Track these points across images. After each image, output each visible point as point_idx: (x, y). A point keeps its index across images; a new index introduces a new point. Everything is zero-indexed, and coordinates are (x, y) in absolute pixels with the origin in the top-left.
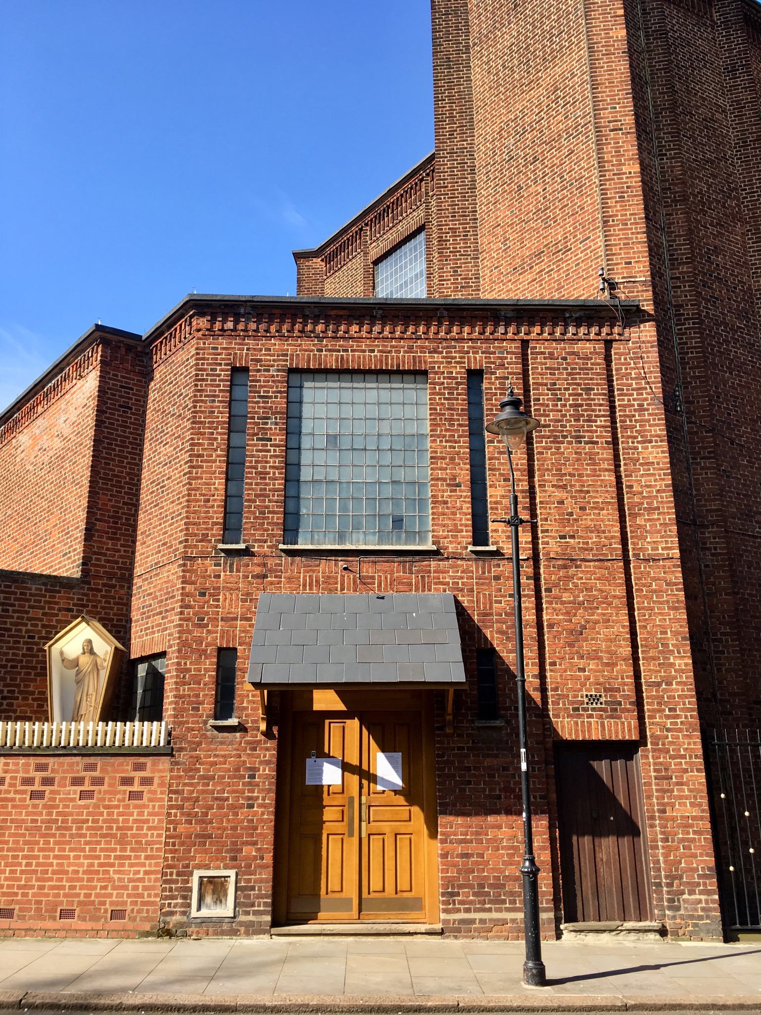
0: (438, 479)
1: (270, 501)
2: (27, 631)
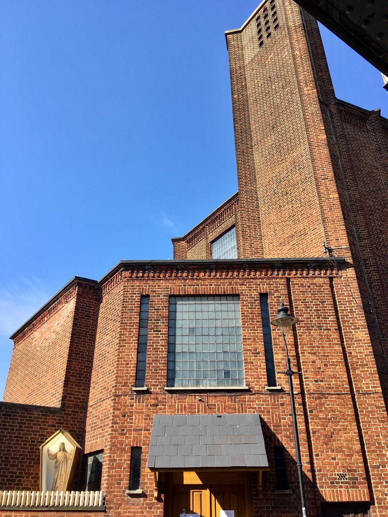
0: (247, 350)
1: (160, 363)
2: (31, 438)
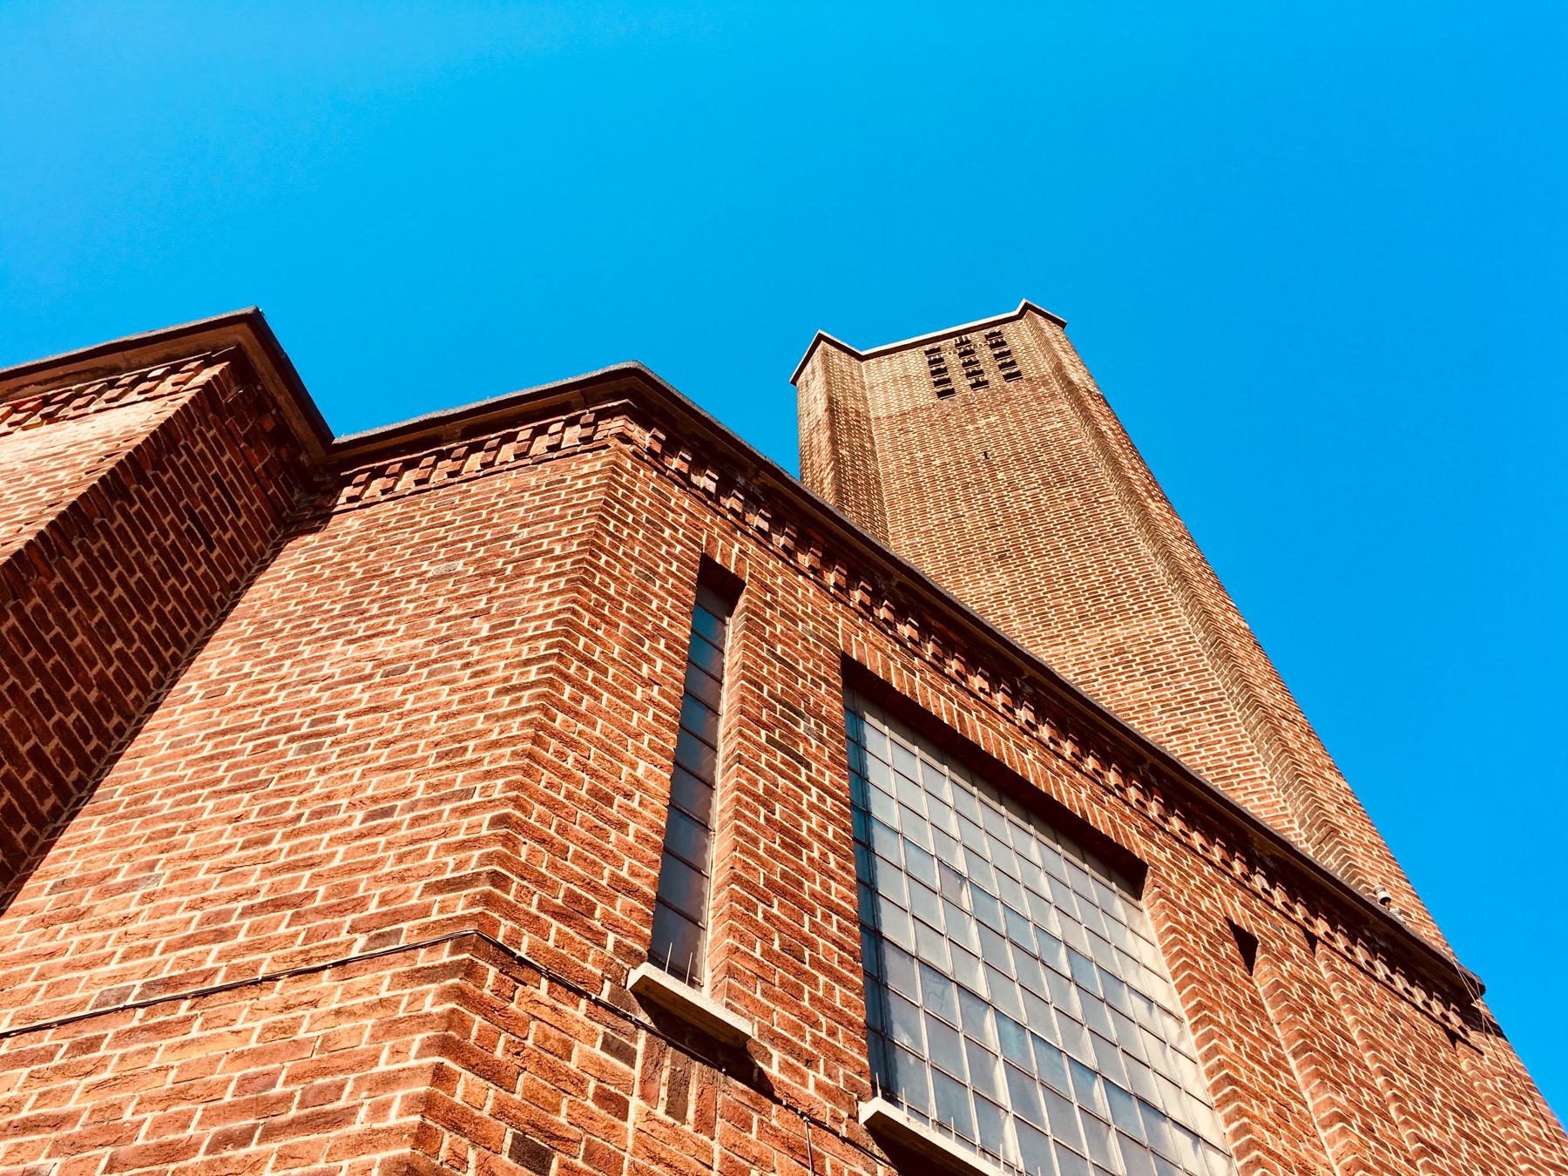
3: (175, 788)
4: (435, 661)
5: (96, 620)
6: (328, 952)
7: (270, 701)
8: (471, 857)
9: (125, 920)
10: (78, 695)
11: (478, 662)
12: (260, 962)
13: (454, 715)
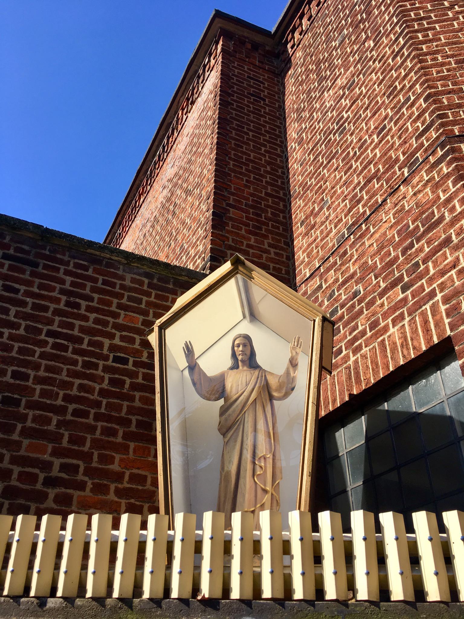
2: (113, 348)
3: (311, 175)
4: (362, 70)
5: (252, 146)
6: (397, 181)
7: (319, 129)
8: (426, 117)
9: (327, 218)
10: (264, 171)
11: (378, 56)
12: (377, 199)
13: (383, 80)
